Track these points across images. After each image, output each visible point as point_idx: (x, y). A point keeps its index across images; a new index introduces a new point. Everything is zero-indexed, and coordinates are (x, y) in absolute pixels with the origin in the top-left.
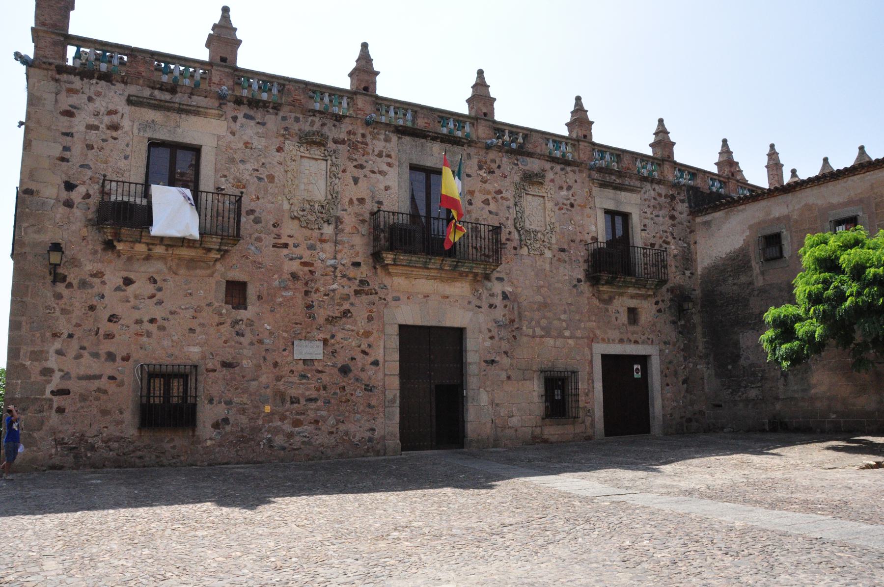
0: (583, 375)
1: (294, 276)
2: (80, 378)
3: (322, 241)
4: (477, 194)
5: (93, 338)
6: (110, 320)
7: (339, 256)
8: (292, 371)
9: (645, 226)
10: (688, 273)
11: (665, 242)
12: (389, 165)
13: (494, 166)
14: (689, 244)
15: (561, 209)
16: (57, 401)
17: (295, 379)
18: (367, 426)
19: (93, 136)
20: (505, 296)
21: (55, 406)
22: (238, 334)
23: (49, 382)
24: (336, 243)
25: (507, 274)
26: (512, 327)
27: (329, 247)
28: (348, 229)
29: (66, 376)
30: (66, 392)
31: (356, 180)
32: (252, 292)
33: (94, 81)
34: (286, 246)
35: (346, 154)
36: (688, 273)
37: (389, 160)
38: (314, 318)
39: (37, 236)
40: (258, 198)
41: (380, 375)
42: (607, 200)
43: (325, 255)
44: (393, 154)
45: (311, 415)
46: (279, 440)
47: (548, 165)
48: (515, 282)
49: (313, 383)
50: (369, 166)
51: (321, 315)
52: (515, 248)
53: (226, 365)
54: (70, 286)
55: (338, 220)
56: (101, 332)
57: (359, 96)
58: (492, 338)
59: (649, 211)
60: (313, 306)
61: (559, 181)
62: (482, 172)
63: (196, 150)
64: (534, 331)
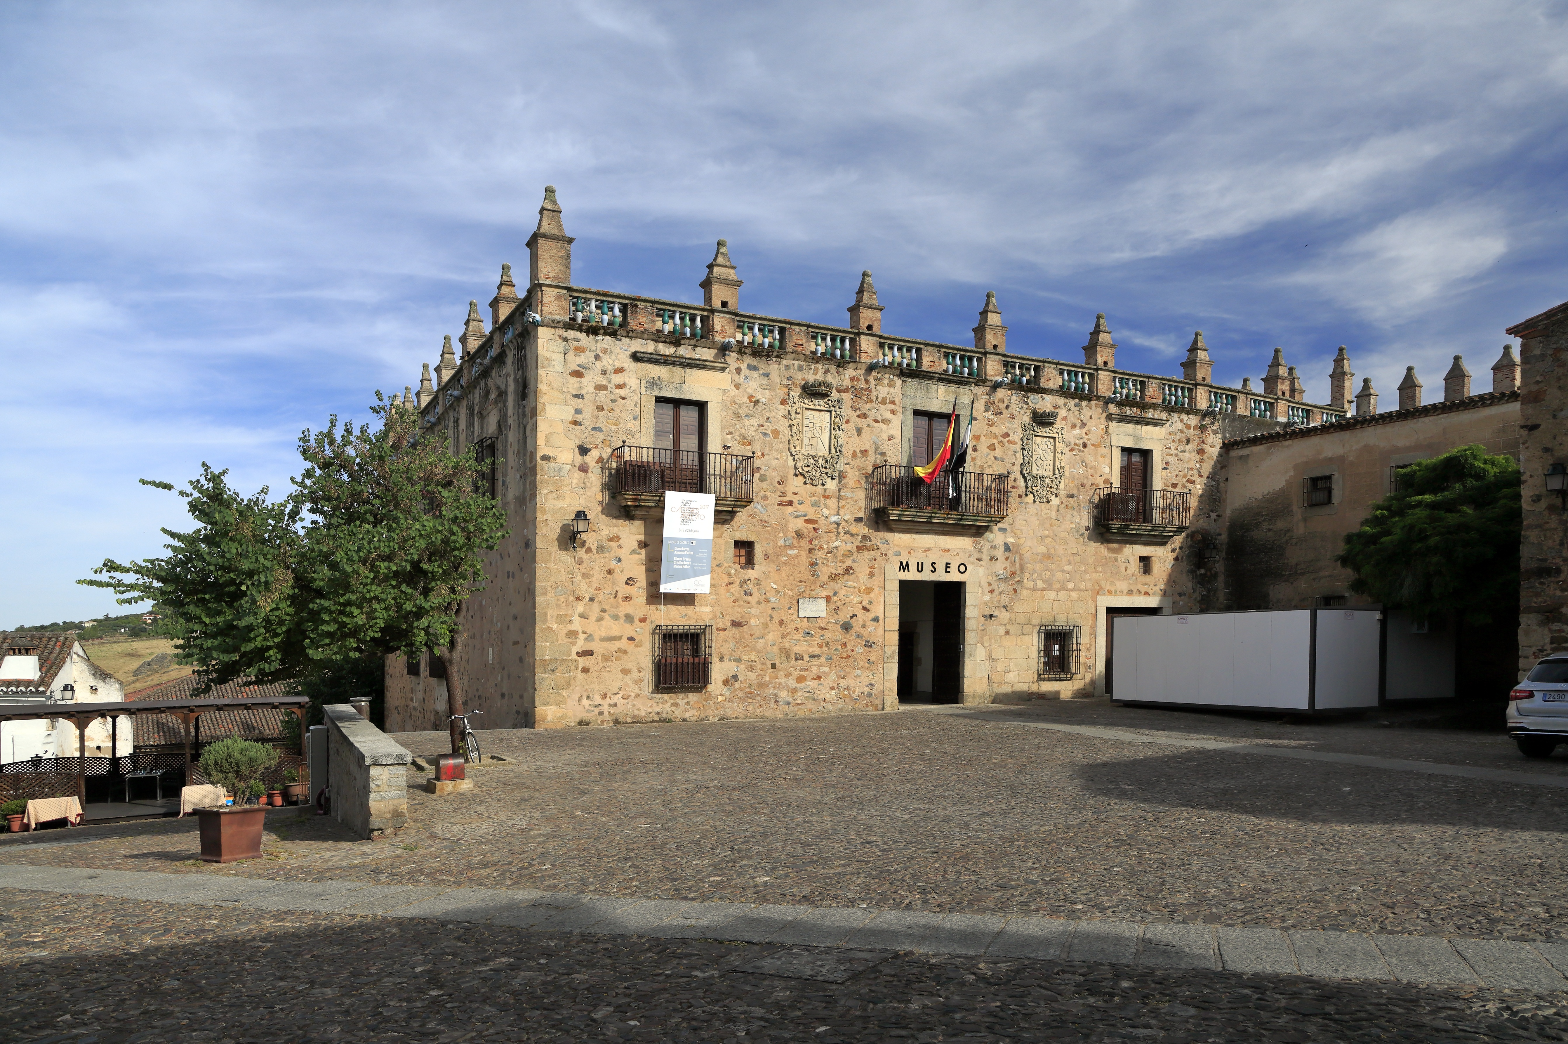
0: (1085, 632)
1: (799, 534)
2: (603, 640)
3: (826, 497)
4: (983, 439)
5: (613, 600)
6: (627, 584)
7: (842, 512)
8: (797, 629)
9: (1167, 463)
10: (1213, 515)
11: (1189, 481)
12: (893, 412)
13: (1002, 406)
14: (1218, 482)
15: (1072, 450)
16: (582, 662)
17: (799, 636)
18: (866, 681)
19: (603, 397)
20: (1007, 548)
21: (580, 667)
22: (746, 593)
23: (574, 644)
24: (839, 498)
25: (1010, 524)
26: (1013, 579)
27: (832, 503)
28: (851, 484)
29: (589, 638)
30: (590, 653)
31: (859, 431)
32: (758, 551)
33: (600, 337)
34: (791, 503)
35: (850, 403)
36: (1213, 515)
37: (892, 407)
38: (818, 576)
39: (556, 503)
40: (763, 455)
41: (880, 631)
42: (1126, 435)
43: (828, 513)
44: (897, 400)
45: (815, 671)
46: (783, 695)
47: (1061, 401)
48: (1018, 532)
49: (817, 640)
50: (872, 414)
51: (825, 572)
52: (1020, 496)
53: (735, 624)
54: (589, 550)
55: (842, 475)
56: (620, 595)
57: (862, 337)
58: (992, 592)
59: (1173, 446)
60: (816, 564)
61: (1072, 419)
62: (989, 414)
63: (701, 406)
64: (1035, 584)
